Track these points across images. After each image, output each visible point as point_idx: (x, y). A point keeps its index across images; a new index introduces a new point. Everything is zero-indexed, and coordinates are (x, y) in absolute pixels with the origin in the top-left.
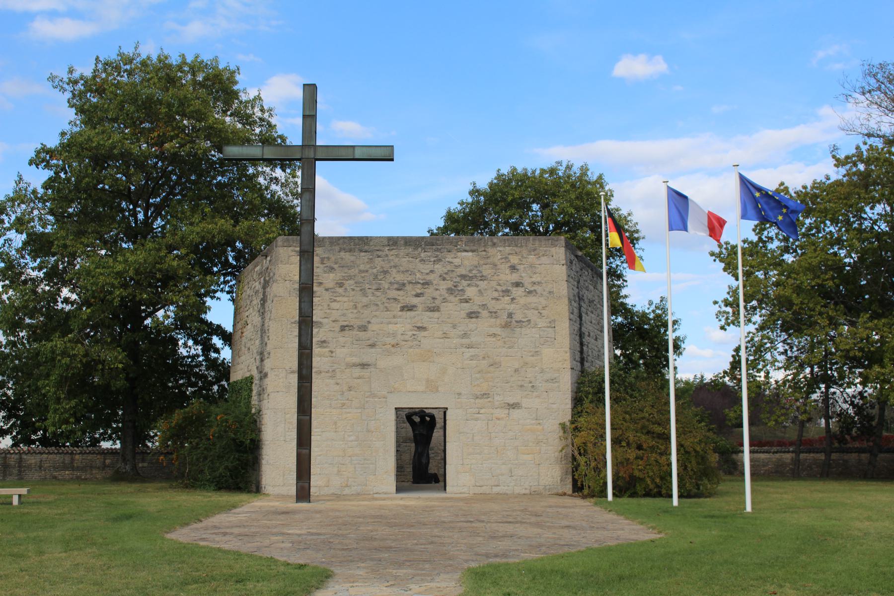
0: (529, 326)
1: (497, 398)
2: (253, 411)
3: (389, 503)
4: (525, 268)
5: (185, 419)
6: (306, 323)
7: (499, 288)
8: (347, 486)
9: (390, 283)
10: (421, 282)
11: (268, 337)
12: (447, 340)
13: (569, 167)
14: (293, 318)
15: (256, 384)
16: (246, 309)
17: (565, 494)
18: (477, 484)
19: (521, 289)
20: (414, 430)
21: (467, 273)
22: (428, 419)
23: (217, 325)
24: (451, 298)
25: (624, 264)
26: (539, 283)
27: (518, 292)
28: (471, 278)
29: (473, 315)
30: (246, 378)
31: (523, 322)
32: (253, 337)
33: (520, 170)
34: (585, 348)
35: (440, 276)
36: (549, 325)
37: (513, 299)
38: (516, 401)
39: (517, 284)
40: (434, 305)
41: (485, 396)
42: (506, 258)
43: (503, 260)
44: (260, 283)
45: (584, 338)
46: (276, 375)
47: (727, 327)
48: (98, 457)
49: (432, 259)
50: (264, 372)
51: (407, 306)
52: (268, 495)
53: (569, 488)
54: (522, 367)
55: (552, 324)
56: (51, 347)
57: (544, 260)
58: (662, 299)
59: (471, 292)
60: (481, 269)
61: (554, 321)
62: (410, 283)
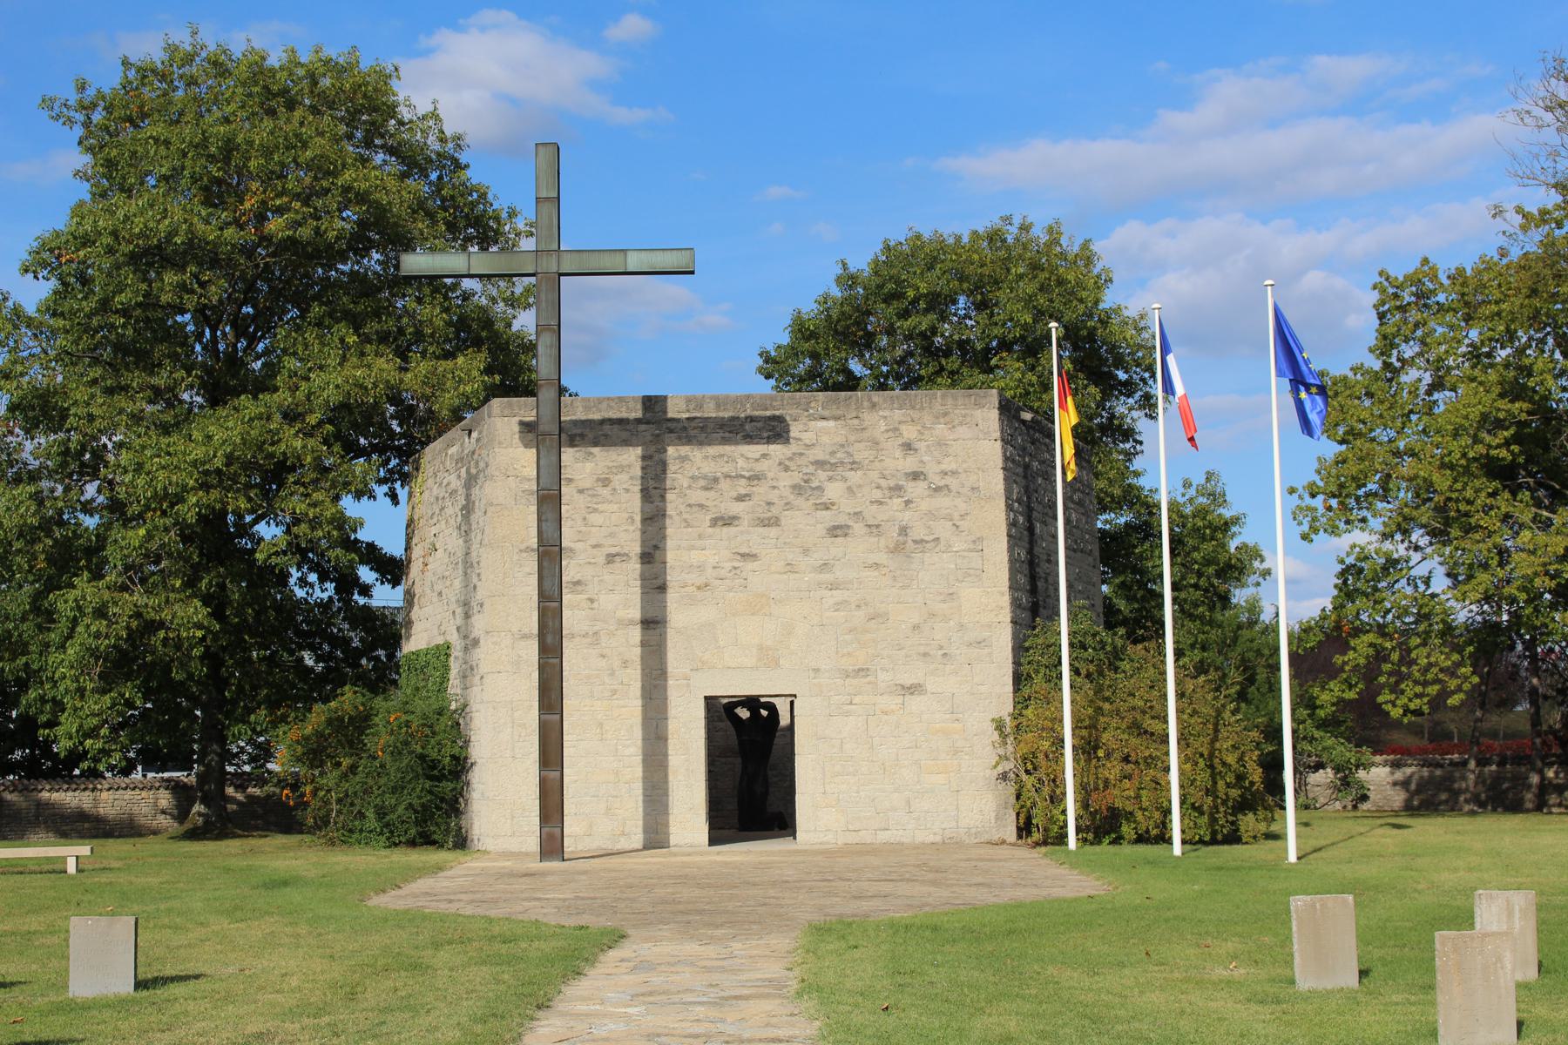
0: (937, 549)
1: (882, 676)
2: (453, 706)
3: (698, 859)
4: (928, 446)
5: (329, 722)
6: (550, 554)
7: (883, 483)
8: (623, 834)
9: (692, 478)
10: (747, 474)
11: (479, 575)
12: (793, 576)
13: (1025, 228)
14: (522, 542)
15: (456, 658)
16: (432, 522)
17: (1003, 842)
18: (851, 827)
19: (922, 485)
20: (739, 734)
21: (827, 457)
22: (764, 713)
23: (367, 544)
24: (800, 502)
25: (1133, 412)
26: (954, 473)
27: (916, 489)
28: (834, 466)
29: (839, 532)
30: (438, 646)
31: (927, 542)
32: (447, 573)
33: (927, 234)
34: (1040, 584)
35: (780, 464)
36: (972, 546)
37: (908, 502)
38: (916, 682)
39: (916, 476)
40: (769, 514)
41: (861, 673)
42: (896, 429)
43: (890, 434)
44: (459, 477)
45: (1038, 565)
46: (495, 643)
47: (1313, 536)
48: (144, 794)
49: (765, 435)
50: (472, 637)
51: (722, 518)
52: (486, 852)
53: (1010, 833)
54: (925, 621)
55: (977, 545)
56: (76, 600)
57: (962, 431)
58: (1209, 476)
59: (834, 491)
60: (850, 450)
61: (981, 539)
62: (727, 476)
